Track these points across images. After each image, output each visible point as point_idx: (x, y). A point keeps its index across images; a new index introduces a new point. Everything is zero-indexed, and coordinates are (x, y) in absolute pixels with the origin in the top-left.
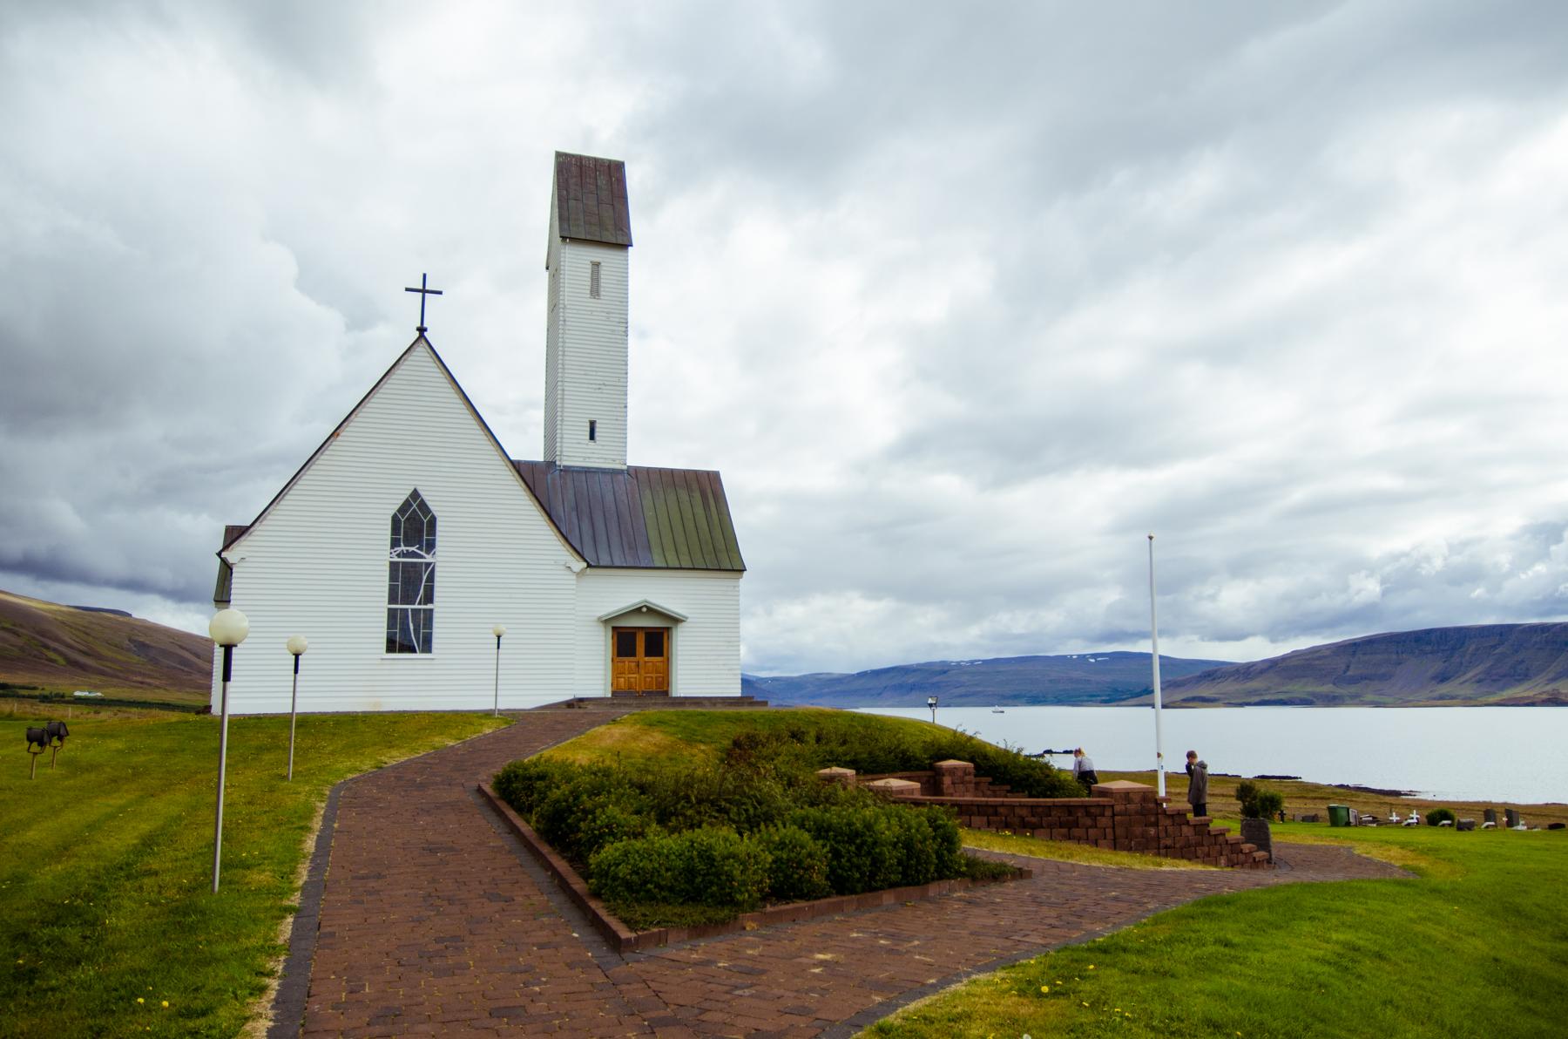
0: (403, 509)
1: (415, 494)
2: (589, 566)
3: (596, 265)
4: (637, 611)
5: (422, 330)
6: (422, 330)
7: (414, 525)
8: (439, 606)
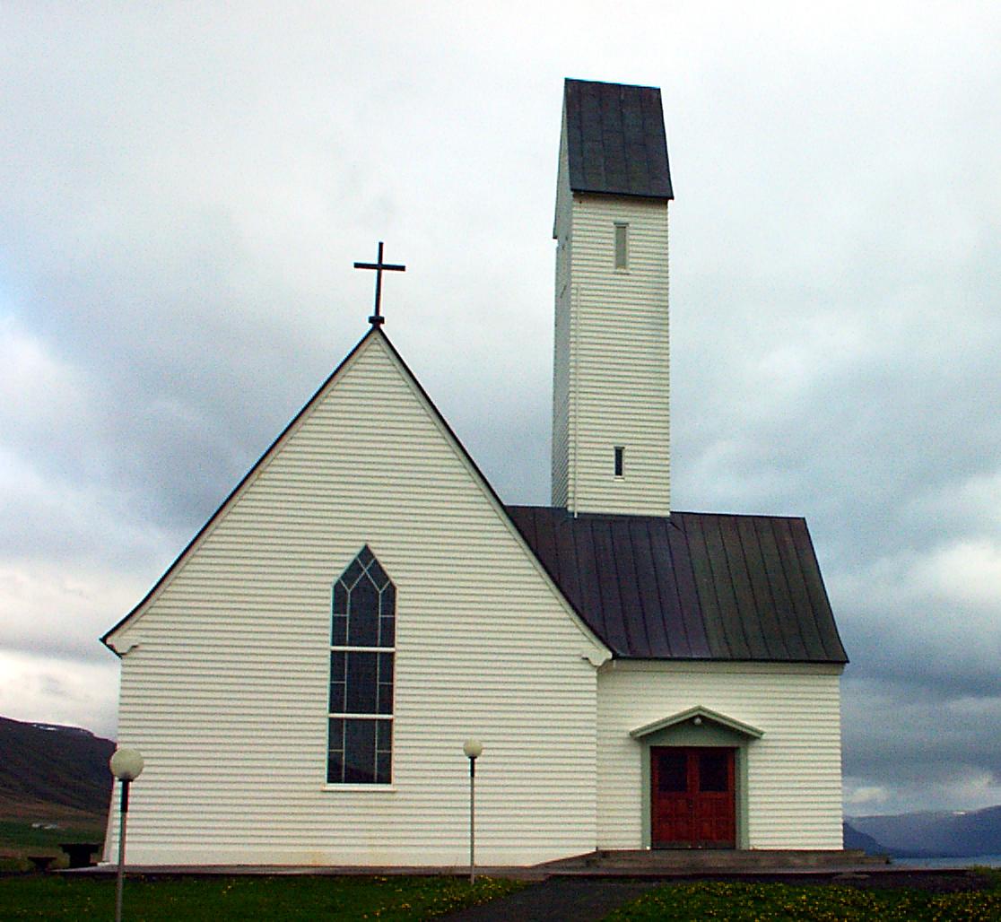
0: (354, 569)
1: (366, 553)
2: (615, 657)
3: (621, 227)
5: (377, 321)
6: (377, 321)
7: (365, 601)
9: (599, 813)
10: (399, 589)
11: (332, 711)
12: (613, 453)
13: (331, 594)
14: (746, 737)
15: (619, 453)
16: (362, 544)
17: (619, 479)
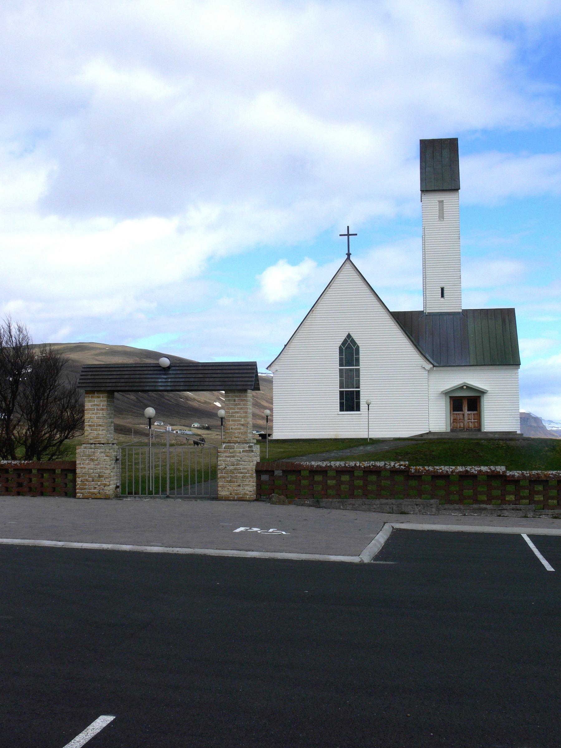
0: (344, 343)
1: (349, 336)
2: (434, 366)
4: (461, 388)
5: (349, 255)
7: (349, 352)
8: (336, 390)
9: (434, 419)
10: (360, 347)
11: (359, 391)
12: (440, 289)
13: (338, 350)
14: (483, 392)
15: (442, 289)
16: (347, 333)
17: (442, 299)
